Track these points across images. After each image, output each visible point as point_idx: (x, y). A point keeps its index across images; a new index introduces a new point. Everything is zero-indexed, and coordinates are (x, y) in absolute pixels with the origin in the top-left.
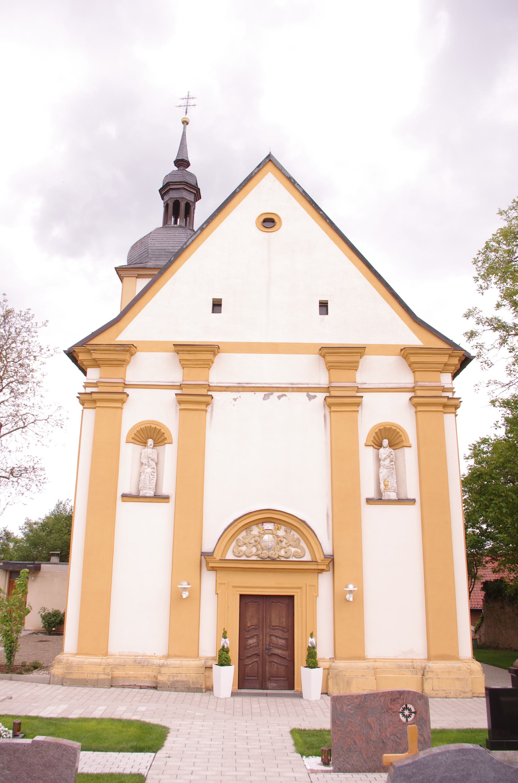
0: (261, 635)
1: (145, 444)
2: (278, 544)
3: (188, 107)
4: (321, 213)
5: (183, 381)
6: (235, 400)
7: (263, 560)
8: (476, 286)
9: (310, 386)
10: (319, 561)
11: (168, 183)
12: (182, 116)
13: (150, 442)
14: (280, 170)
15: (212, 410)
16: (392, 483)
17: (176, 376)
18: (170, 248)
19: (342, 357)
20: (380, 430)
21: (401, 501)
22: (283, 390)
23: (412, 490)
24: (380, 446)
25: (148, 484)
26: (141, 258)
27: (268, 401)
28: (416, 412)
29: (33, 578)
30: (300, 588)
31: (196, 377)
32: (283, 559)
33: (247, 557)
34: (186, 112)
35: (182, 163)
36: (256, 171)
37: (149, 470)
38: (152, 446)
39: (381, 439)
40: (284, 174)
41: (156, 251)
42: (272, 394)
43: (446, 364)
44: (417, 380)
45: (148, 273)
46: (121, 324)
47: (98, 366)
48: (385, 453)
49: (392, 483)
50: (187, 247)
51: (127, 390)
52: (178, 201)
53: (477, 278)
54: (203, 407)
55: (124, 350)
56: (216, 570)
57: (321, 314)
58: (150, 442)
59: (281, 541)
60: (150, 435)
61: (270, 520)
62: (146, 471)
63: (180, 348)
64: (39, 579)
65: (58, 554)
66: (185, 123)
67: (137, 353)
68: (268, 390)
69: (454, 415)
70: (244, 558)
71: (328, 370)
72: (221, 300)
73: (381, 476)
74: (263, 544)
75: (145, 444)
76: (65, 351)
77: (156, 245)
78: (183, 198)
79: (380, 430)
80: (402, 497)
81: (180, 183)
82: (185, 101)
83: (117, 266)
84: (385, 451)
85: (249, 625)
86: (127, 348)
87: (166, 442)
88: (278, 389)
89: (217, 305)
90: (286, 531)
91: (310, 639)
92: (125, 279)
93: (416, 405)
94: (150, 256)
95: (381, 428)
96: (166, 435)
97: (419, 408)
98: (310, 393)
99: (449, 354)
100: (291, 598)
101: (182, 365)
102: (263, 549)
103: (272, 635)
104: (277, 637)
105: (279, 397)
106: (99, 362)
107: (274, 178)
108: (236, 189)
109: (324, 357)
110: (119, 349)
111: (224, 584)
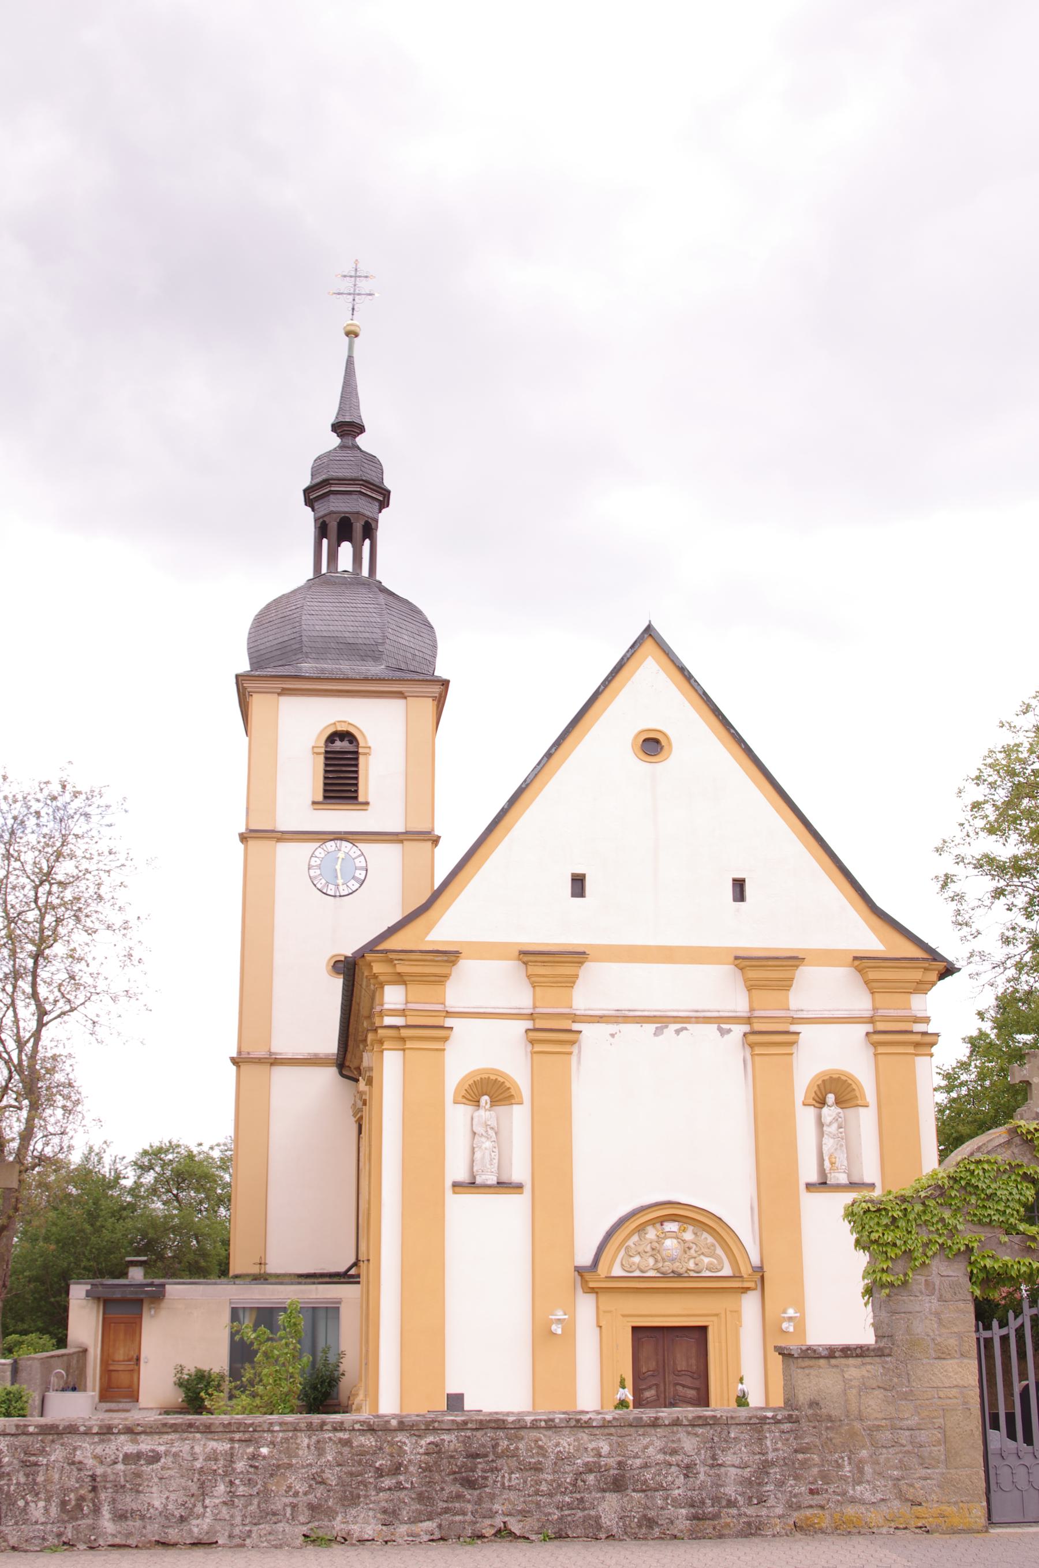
0: (662, 1385)
1: (477, 1103)
2: (685, 1252)
3: (357, 297)
6: (613, 1035)
7: (664, 1276)
9: (722, 1014)
10: (745, 1276)
12: (346, 320)
13: (485, 1099)
14: (667, 655)
15: (580, 1052)
16: (841, 1159)
17: (522, 998)
18: (347, 635)
19: (767, 971)
20: (824, 1081)
21: (504, 1186)
22: (684, 1020)
23: (519, 1171)
24: (822, 1103)
27: (661, 1037)
28: (875, 1055)
29: (153, 1312)
30: (717, 1315)
31: (551, 1003)
32: (692, 1274)
33: (642, 1272)
35: (348, 428)
37: (488, 1144)
38: (488, 1106)
42: (667, 1027)
44: (878, 1006)
46: (431, 913)
48: (830, 1115)
49: (841, 1159)
50: (528, 785)
52: (348, 519)
55: (446, 961)
56: (597, 1293)
57: (735, 900)
58: (485, 1099)
59: (689, 1248)
60: (489, 1090)
61: (673, 1218)
63: (528, 956)
64: (163, 1313)
66: (352, 334)
68: (661, 1021)
70: (637, 1273)
73: (825, 1149)
74: (664, 1253)
75: (477, 1103)
78: (358, 513)
79: (824, 1081)
80: (856, 1180)
81: (353, 481)
85: (644, 1370)
88: (676, 1019)
89: (579, 884)
90: (695, 1234)
91: (740, 1386)
94: (305, 649)
95: (825, 1078)
97: (881, 1050)
99: (926, 969)
100: (703, 1330)
102: (664, 1260)
103: (678, 1384)
104: (684, 1386)
105: (678, 1032)
106: (406, 978)
107: (658, 668)
109: (741, 969)
111: (610, 1312)
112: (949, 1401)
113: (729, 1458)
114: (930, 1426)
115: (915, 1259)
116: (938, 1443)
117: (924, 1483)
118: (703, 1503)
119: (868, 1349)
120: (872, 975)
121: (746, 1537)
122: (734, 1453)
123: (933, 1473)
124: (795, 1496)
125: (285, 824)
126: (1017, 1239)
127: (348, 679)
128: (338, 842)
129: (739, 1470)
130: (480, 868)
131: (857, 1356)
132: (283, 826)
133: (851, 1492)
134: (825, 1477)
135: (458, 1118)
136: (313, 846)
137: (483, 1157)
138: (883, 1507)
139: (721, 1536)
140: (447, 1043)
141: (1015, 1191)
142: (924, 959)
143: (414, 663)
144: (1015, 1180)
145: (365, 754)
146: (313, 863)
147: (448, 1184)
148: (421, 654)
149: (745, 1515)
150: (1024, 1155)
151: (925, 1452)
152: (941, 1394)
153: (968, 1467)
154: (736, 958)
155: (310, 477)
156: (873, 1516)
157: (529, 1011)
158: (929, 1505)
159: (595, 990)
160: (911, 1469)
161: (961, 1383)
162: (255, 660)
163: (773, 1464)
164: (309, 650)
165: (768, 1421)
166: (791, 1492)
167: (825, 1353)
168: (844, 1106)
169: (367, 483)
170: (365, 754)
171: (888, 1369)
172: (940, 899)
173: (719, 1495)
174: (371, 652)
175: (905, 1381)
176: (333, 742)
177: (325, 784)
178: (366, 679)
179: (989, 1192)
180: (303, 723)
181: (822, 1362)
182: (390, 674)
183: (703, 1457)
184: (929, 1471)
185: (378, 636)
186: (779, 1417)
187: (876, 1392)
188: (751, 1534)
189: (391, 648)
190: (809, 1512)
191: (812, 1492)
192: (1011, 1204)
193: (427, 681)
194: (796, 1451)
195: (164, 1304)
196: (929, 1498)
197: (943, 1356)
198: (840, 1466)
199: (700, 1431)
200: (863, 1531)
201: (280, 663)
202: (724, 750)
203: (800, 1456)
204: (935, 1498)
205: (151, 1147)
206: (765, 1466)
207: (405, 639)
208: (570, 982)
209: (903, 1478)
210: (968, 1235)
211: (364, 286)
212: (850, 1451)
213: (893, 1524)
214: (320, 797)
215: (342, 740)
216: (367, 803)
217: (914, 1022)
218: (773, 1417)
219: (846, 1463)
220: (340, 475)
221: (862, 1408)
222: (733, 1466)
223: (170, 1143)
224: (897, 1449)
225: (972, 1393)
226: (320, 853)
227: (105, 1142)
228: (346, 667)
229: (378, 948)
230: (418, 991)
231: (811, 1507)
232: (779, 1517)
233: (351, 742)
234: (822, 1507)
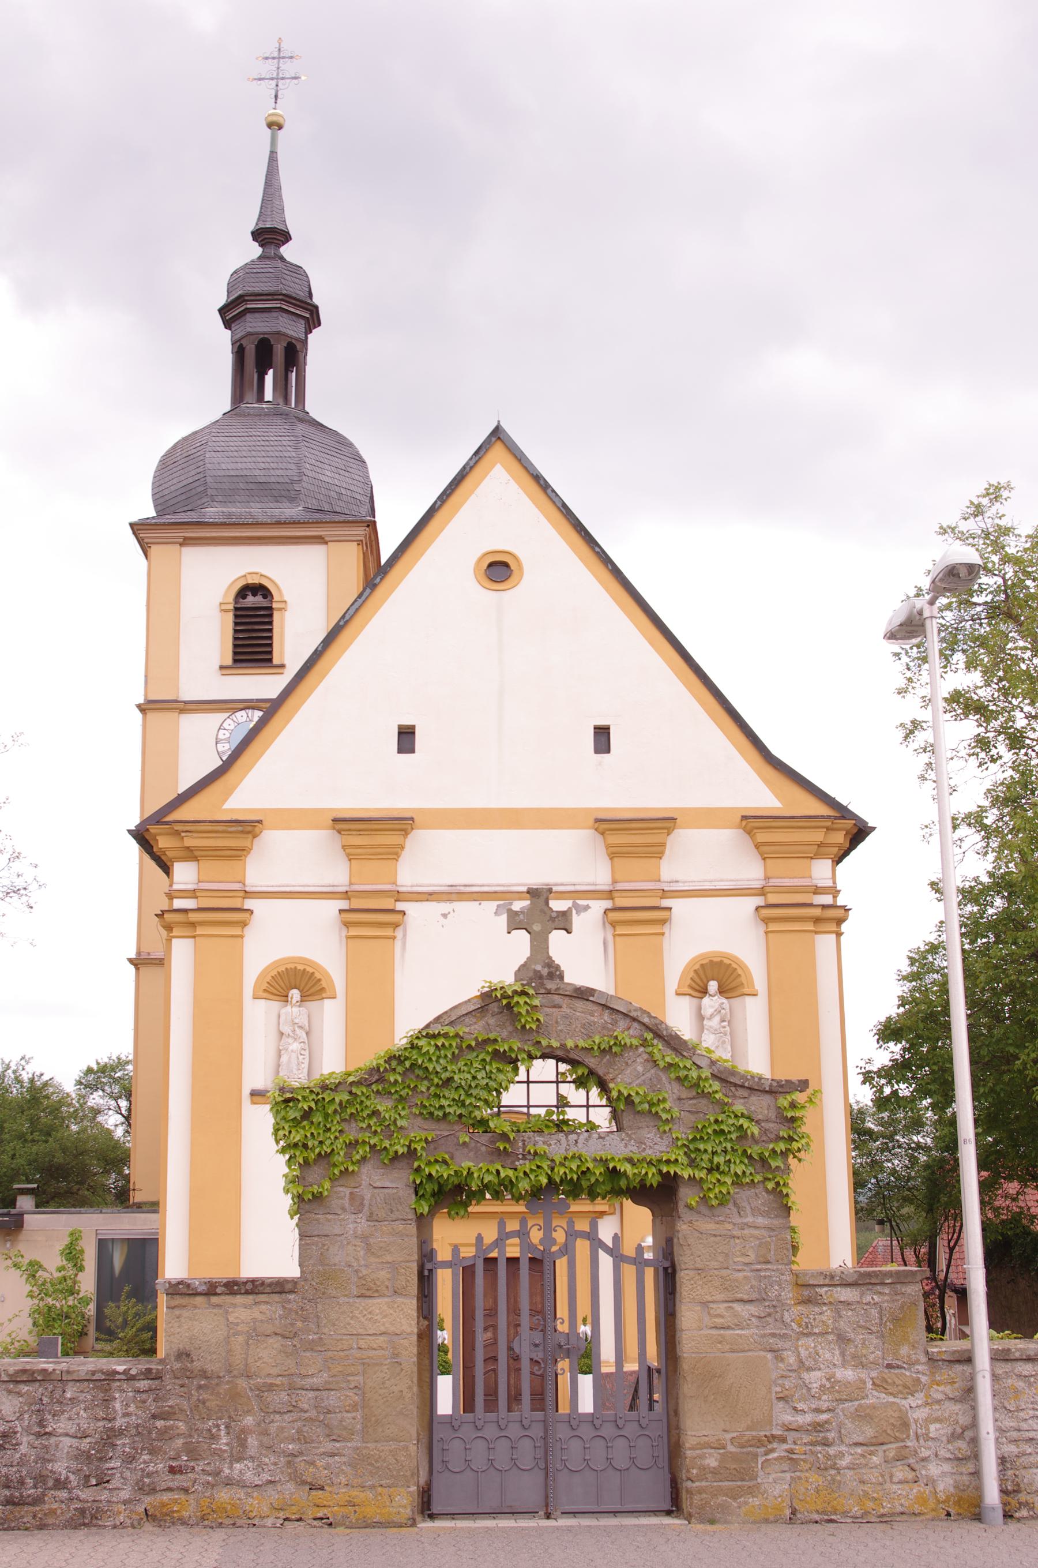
1: (285, 998)
3: (281, 82)
4: (597, 549)
5: (351, 884)
6: (445, 916)
8: (1012, 494)
11: (240, 297)
12: (268, 109)
13: (295, 994)
14: (519, 461)
15: (405, 935)
18: (257, 472)
19: (634, 836)
24: (704, 992)
25: (295, 1071)
26: (188, 495)
28: (766, 933)
31: (372, 877)
34: (276, 97)
35: (271, 236)
36: (472, 464)
37: (295, 1046)
39: (705, 981)
40: (526, 468)
41: (225, 479)
43: (820, 845)
44: (769, 875)
45: (208, 535)
47: (195, 859)
48: (712, 1007)
50: (346, 622)
51: (249, 904)
53: (899, 654)
54: (388, 932)
55: (242, 832)
58: (295, 994)
62: (291, 1048)
65: (33, 1189)
66: (275, 125)
67: (265, 832)
69: (834, 936)
71: (611, 859)
72: (413, 727)
75: (285, 998)
76: (129, 831)
77: (224, 466)
78: (278, 333)
79: (702, 965)
81: (272, 296)
82: (271, 65)
83: (135, 519)
84: (712, 1003)
86: (249, 829)
87: (324, 995)
89: (406, 738)
92: (154, 550)
93: (766, 921)
94: (210, 492)
95: (704, 962)
96: (324, 984)
97: (772, 927)
98: (578, 902)
99: (828, 829)
101: (348, 855)
106: (197, 853)
108: (435, 502)
109: (602, 834)
110: (233, 829)
112: (372, 1353)
113: (62, 1425)
114: (344, 1385)
115: (335, 1165)
116: (354, 1407)
117: (330, 1460)
118: (22, 1482)
119: (263, 1284)
120: (761, 837)
121: (75, 1528)
122: (70, 1419)
123: (344, 1447)
124: (149, 1475)
125: (189, 692)
126: (485, 1138)
127: (257, 524)
128: (250, 712)
129: (74, 1440)
130: (288, 722)
131: (247, 1293)
132: (186, 695)
133: (227, 1471)
134: (193, 1453)
135: (259, 1017)
136: (222, 716)
137: (289, 1061)
138: (270, 1490)
139: (42, 1527)
140: (246, 929)
141: (481, 1075)
142: (829, 817)
143: (341, 503)
144: (484, 1060)
145: (280, 609)
146: (221, 736)
147: (246, 1092)
148: (349, 493)
149: (78, 1499)
150: (502, 1026)
151: (334, 1419)
152: (362, 1344)
153: (393, 1440)
154: (597, 820)
155: (226, 293)
156: (256, 1503)
157: (344, 889)
158: (335, 1489)
159: (422, 863)
160: (312, 1441)
161: (392, 1329)
162: (160, 508)
163: (121, 1433)
164: (214, 492)
165: (118, 1377)
166: (143, 1470)
167: (202, 1288)
168: (730, 995)
169: (288, 298)
170: (280, 609)
171: (290, 1310)
172: (906, 753)
173: (44, 1473)
174: (286, 493)
175: (312, 1326)
176: (244, 597)
177: (235, 646)
178: (279, 523)
179: (444, 1076)
180: (212, 575)
181: (199, 1300)
182: (308, 516)
183: (26, 1423)
184: (338, 1445)
185: (293, 472)
186: (133, 1372)
187: (271, 1340)
188: (84, 1524)
189: (310, 487)
190: (166, 1497)
191: (172, 1470)
192: (474, 1092)
193: (349, 522)
194: (154, 1417)
195: (24, 1235)
196: (336, 1481)
197: (369, 1293)
198: (214, 1438)
199: (25, 1388)
200: (239, 1522)
201: (186, 509)
202: (429, 552)
203: (160, 1424)
204: (344, 1481)
205: (98, 1063)
206: (110, 1437)
207: (328, 475)
208: (394, 853)
209: (301, 1453)
210: (416, 1132)
211: (288, 68)
212: (230, 1417)
213: (282, 1515)
214: (229, 661)
215: (254, 595)
216: (283, 666)
217: (815, 893)
218: (125, 1372)
219: (223, 1433)
220: (257, 290)
221: (250, 1360)
222: (67, 1435)
223: (119, 1059)
224: (295, 1415)
225: (406, 1343)
226: (230, 725)
227: (23, 1058)
228: (257, 510)
229: (167, 819)
230: (213, 867)
231: (169, 1489)
232: (125, 1502)
233: (265, 597)
234: (186, 1490)
